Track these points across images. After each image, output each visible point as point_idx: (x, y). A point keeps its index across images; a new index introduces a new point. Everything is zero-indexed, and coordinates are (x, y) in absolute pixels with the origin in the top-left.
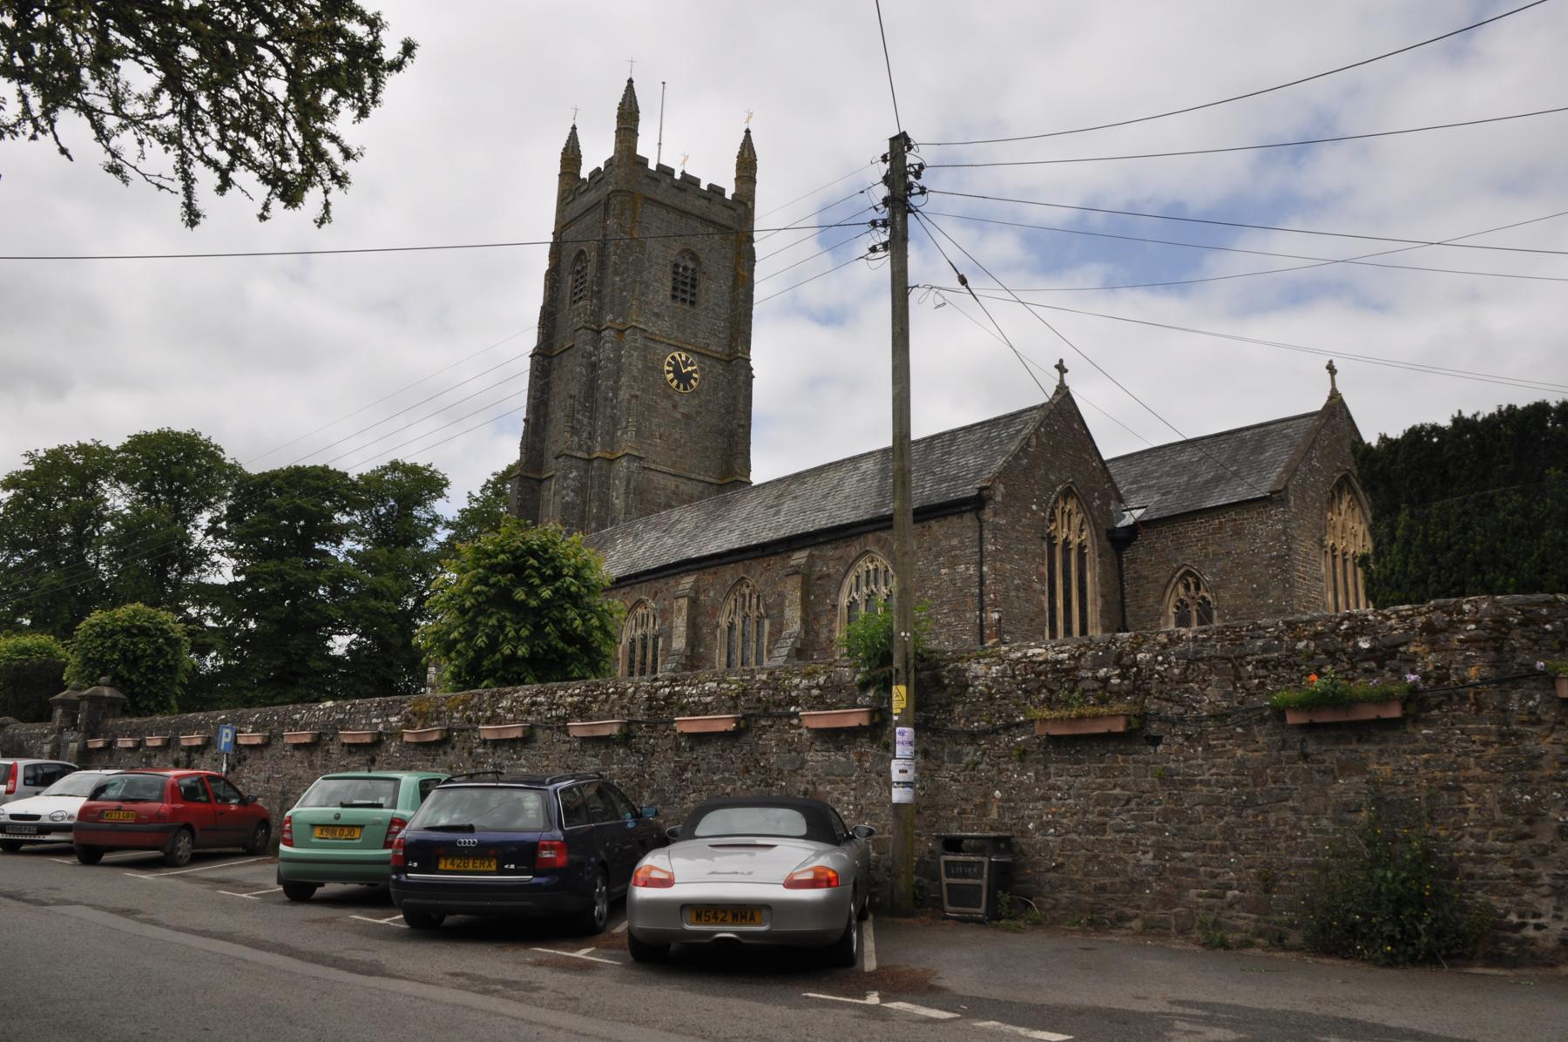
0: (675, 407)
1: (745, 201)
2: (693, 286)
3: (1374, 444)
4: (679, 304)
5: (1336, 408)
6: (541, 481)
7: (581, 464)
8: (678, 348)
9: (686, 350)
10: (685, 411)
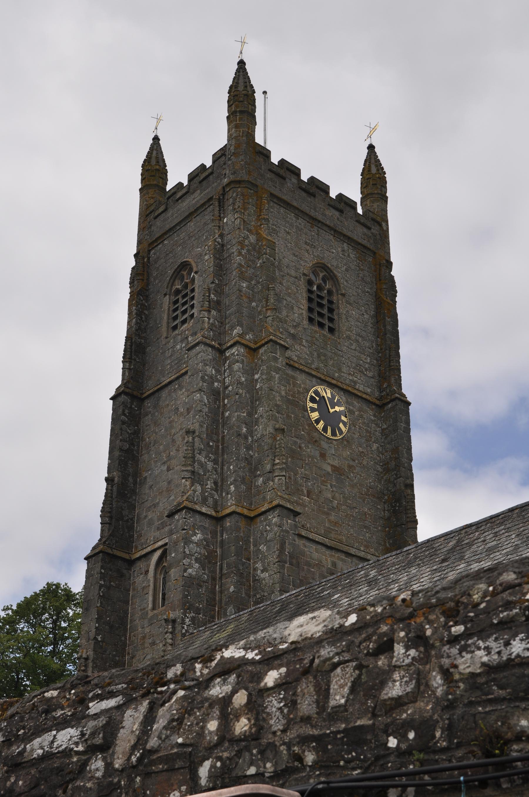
0: (323, 456)
1: (375, 221)
2: (331, 310)
4: (316, 328)
6: (131, 563)
7: (207, 523)
8: (323, 382)
10: (336, 463)
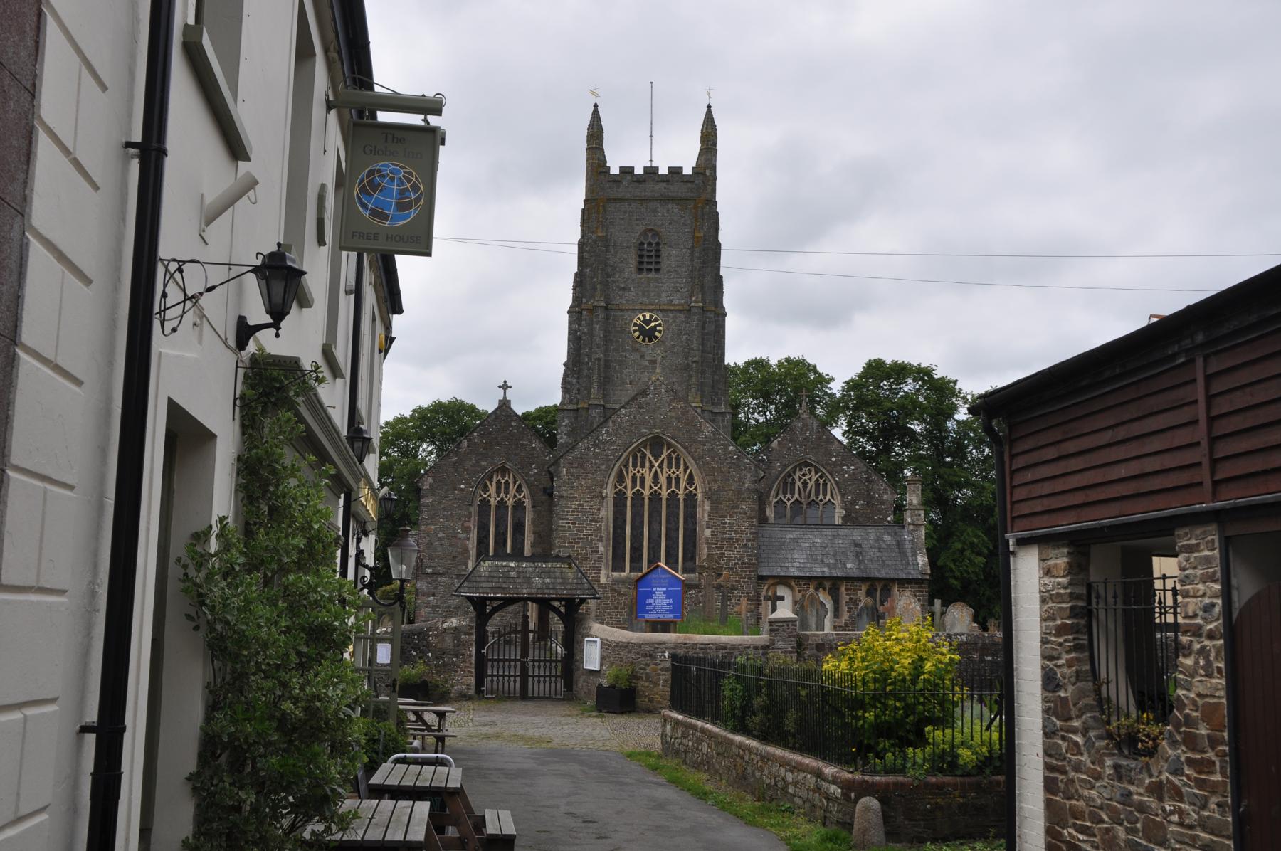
0: (642, 357)
2: (658, 256)
3: (615, 171)
5: (505, 404)
7: (571, 414)
9: (649, 311)
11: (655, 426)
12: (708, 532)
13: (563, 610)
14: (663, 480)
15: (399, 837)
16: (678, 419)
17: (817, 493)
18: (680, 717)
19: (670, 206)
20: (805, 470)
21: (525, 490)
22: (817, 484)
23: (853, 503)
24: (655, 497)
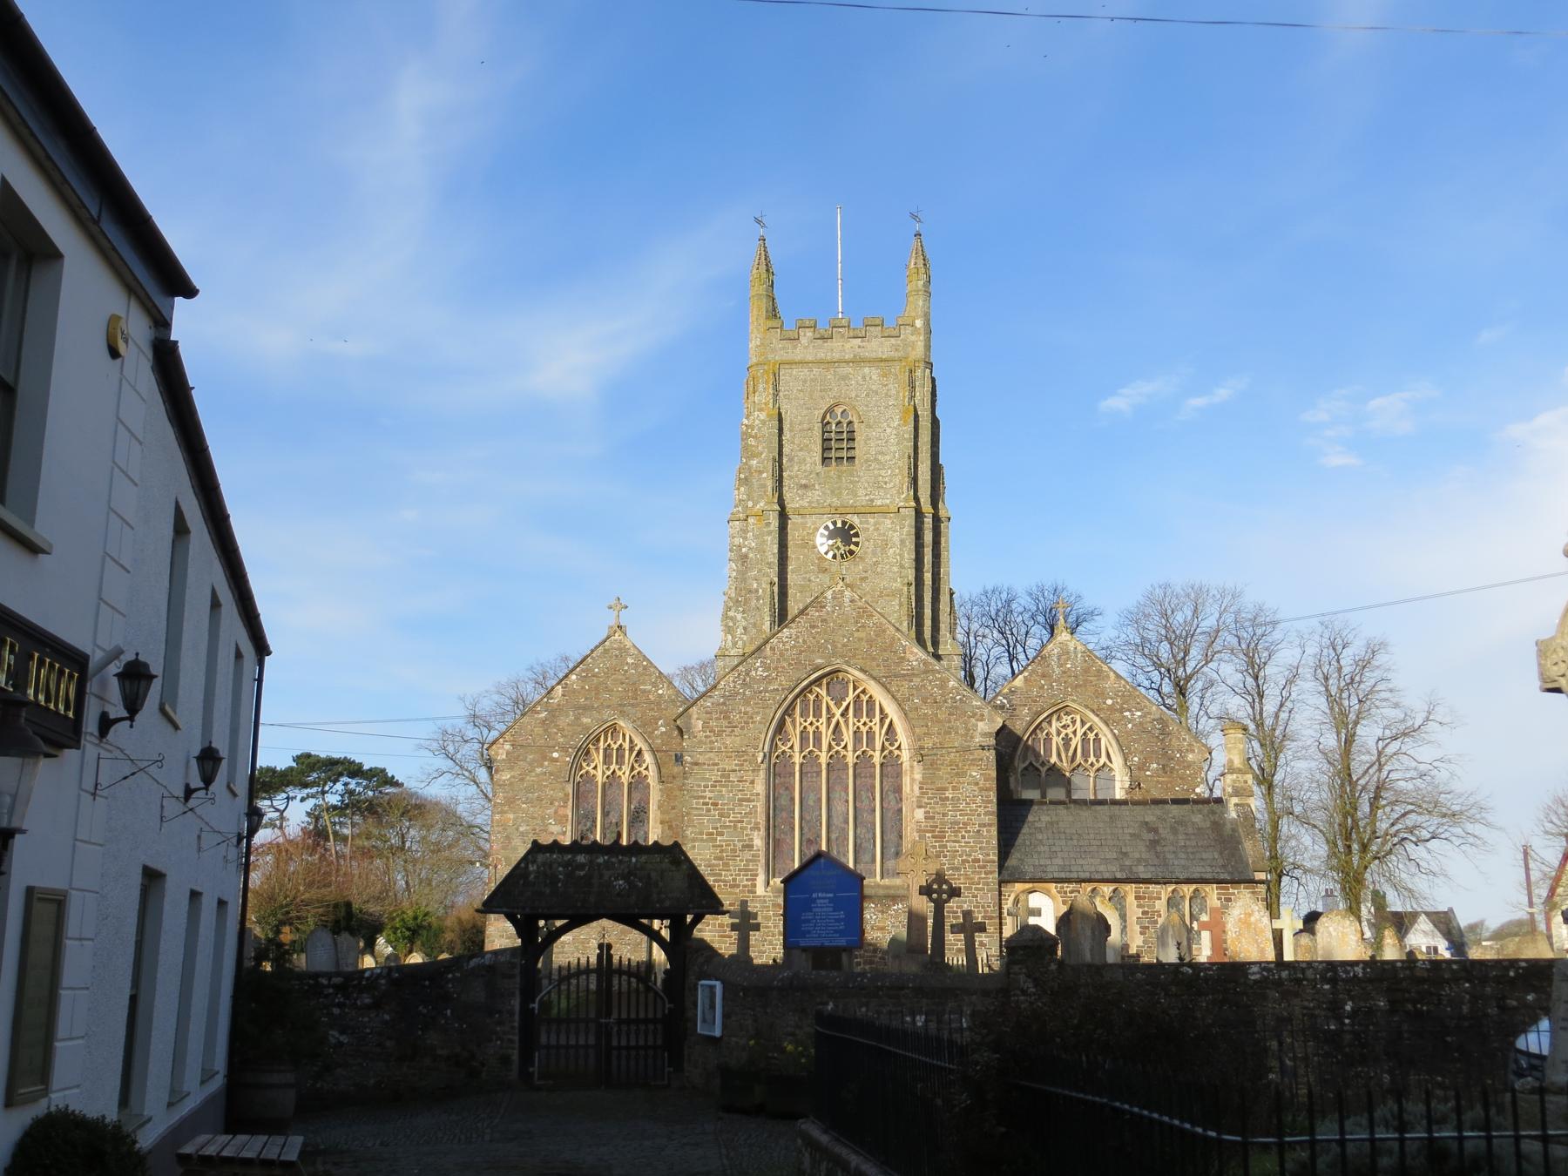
11: (834, 654)
12: (920, 814)
13: (665, 933)
14: (848, 737)
15: (1171, 956)
16: (870, 642)
17: (1085, 755)
18: (824, 1139)
19: (867, 370)
20: (1066, 720)
21: (648, 758)
22: (1085, 740)
23: (1142, 767)
24: (836, 764)
